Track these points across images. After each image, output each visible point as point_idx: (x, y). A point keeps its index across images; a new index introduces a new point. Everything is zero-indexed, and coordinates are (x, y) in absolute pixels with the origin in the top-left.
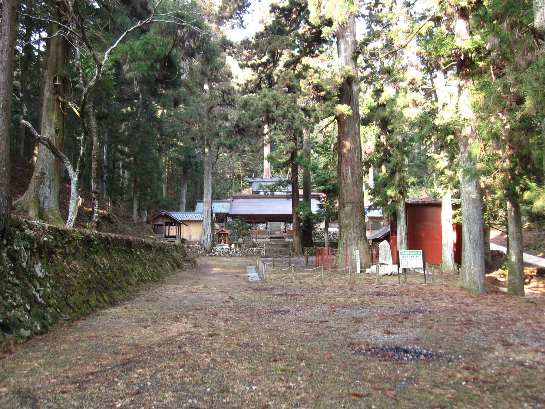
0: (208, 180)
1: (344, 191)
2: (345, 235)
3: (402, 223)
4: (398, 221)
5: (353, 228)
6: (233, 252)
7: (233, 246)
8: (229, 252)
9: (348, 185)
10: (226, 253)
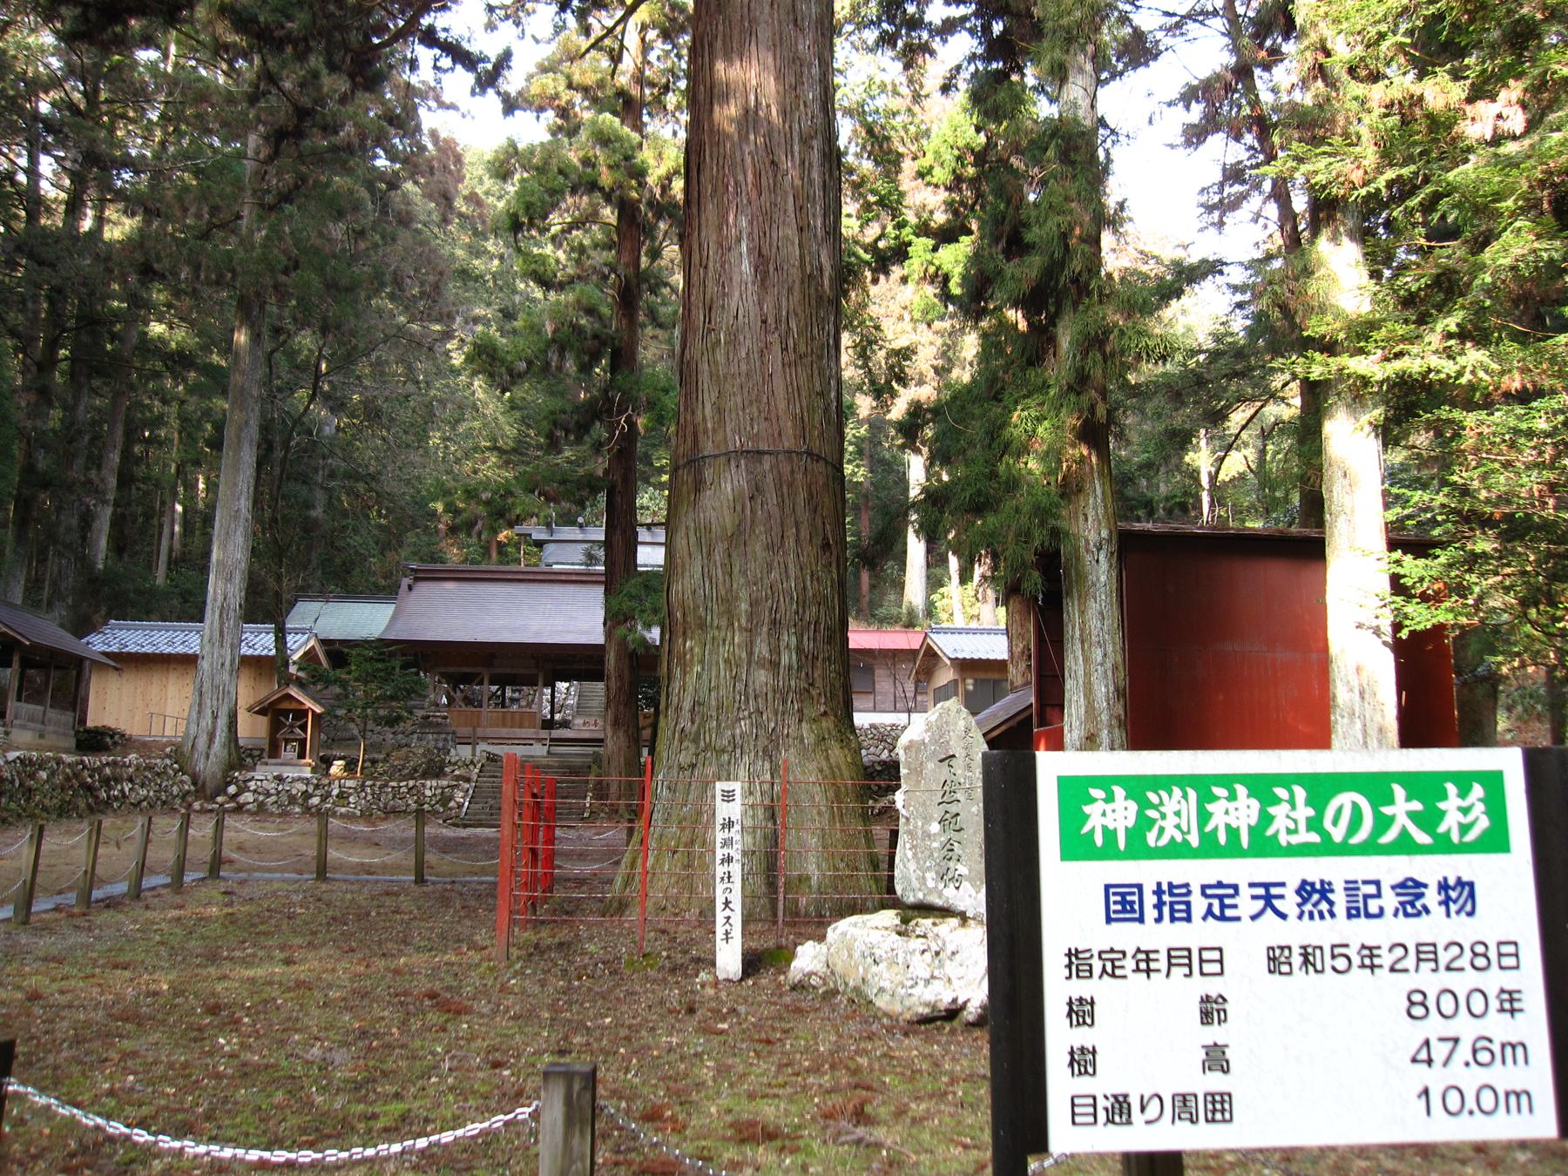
0: (236, 468)
1: (704, 378)
2: (691, 679)
3: (1094, 623)
4: (1072, 611)
5: (751, 631)
6: (324, 798)
7: (337, 768)
8: (307, 796)
9: (733, 341)
10: (292, 800)
